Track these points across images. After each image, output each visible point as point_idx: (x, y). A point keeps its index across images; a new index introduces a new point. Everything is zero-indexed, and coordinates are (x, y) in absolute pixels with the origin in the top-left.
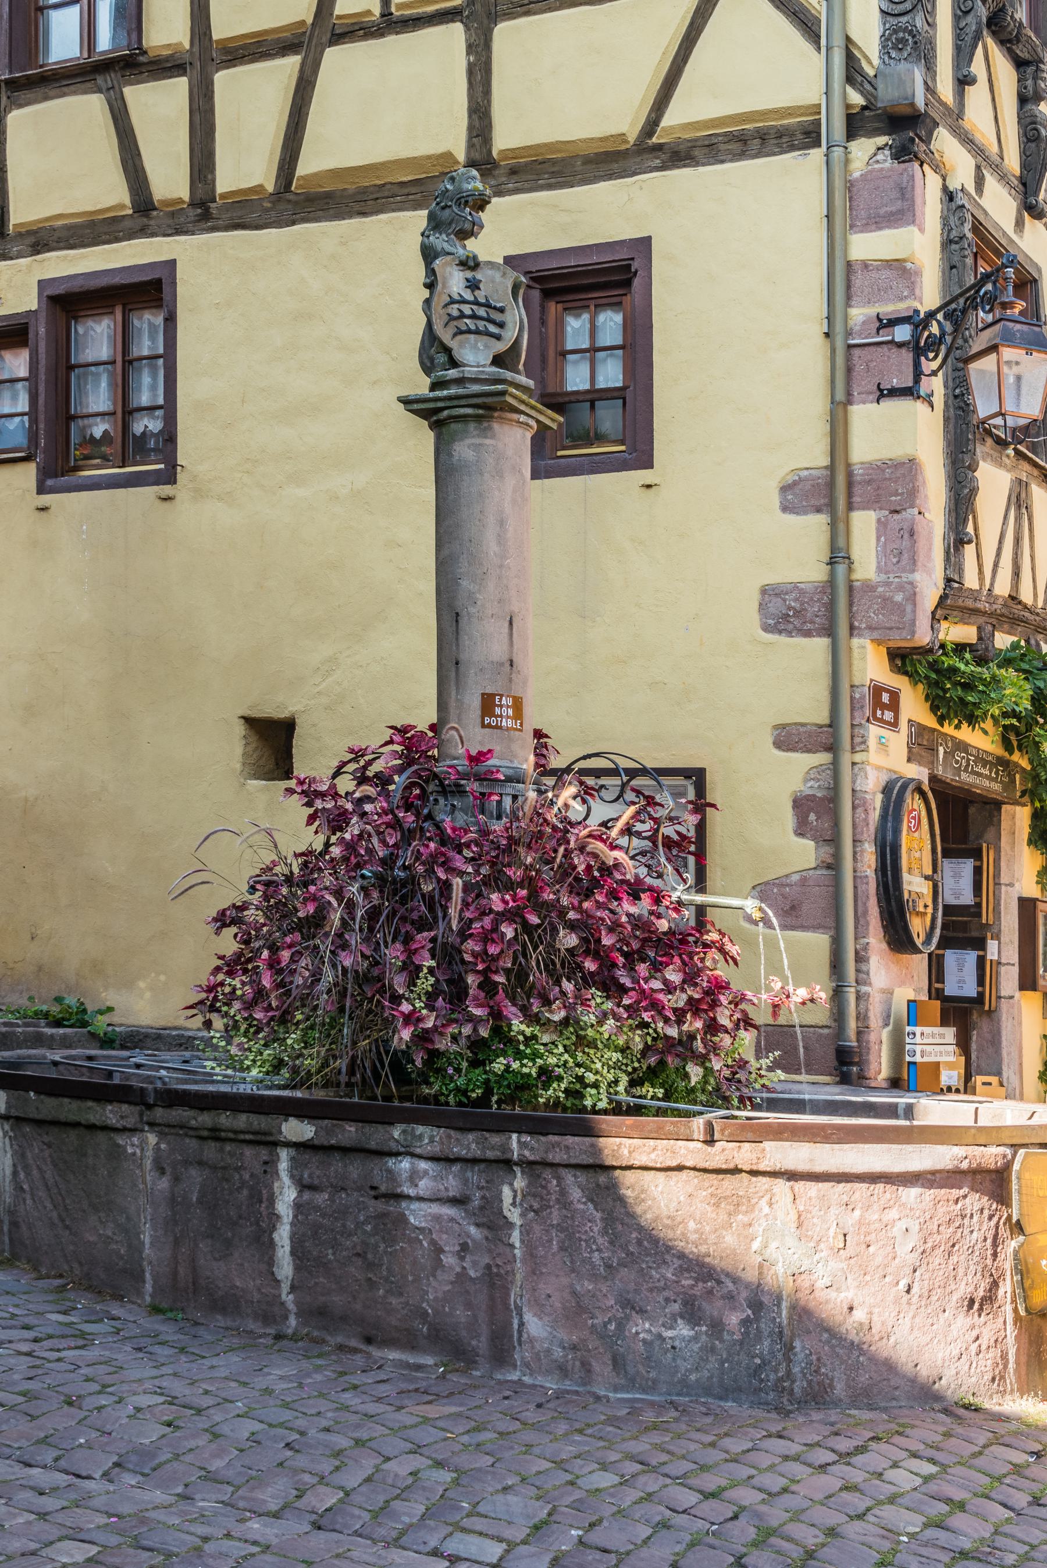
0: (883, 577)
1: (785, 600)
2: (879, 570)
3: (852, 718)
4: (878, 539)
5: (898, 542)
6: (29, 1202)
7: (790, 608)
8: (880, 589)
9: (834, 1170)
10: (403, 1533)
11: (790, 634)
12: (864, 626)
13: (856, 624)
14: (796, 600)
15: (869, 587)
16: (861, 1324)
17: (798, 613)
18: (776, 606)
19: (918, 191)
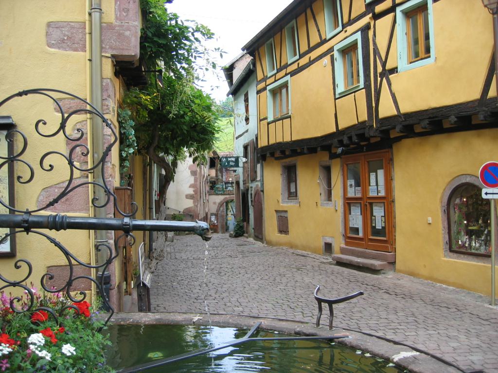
0: (118, 23)
1: (62, 31)
2: (117, 18)
3: (102, 96)
4: (116, 3)
5: (127, 4)
6: (369, 344)
7: (65, 35)
8: (117, 28)
9: (443, 363)
10: (118, 365)
11: (65, 49)
12: (107, 47)
13: (104, 46)
14: (68, 31)
15: (110, 26)
16: (14, 362)
17: (69, 38)
18: (56, 34)
19: (262, 196)
